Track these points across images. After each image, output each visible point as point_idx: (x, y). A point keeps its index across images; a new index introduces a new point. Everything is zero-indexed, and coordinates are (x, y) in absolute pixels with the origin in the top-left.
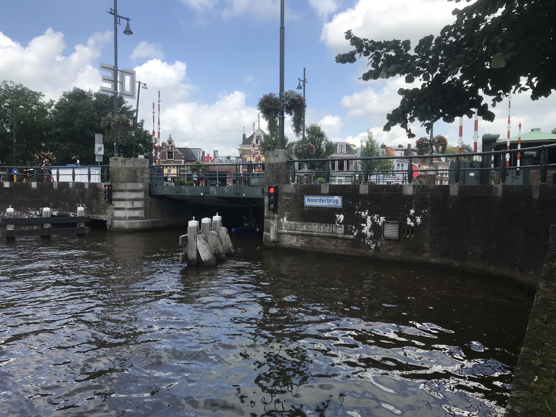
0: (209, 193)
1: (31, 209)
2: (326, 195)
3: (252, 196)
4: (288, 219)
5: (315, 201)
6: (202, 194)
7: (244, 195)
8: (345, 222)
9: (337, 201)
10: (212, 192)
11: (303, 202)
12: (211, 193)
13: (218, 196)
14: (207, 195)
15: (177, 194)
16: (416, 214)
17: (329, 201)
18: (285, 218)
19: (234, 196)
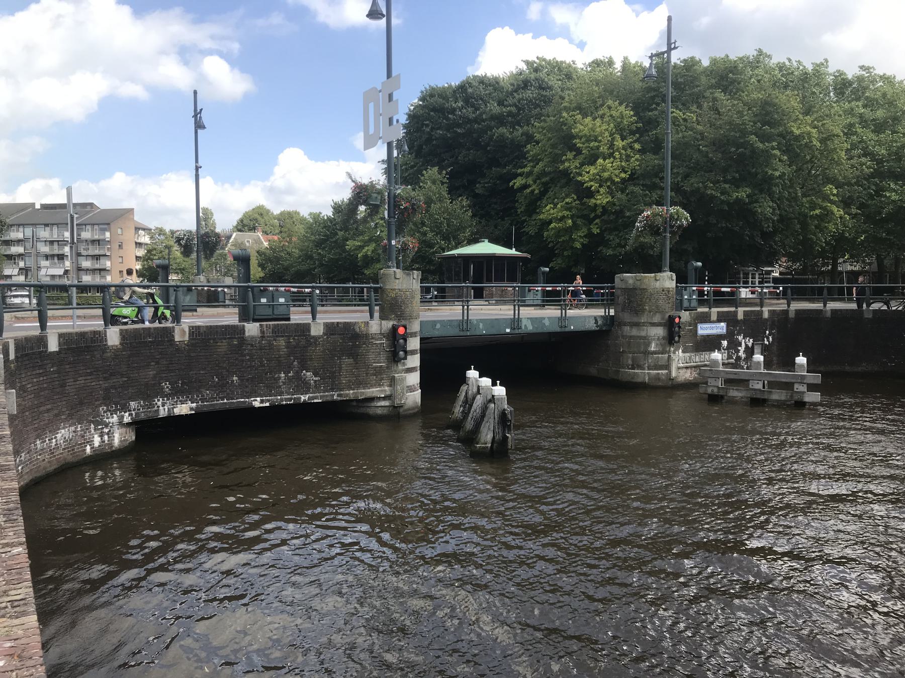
0: (521, 328)
1: (108, 410)
2: (714, 322)
3: (583, 329)
4: (683, 352)
5: (706, 329)
6: (508, 330)
7: (572, 327)
8: (728, 348)
9: (702, 328)
10: (526, 326)
11: (696, 331)
12: (523, 328)
13: (535, 331)
14: (517, 331)
15: (462, 334)
16: (770, 334)
17: (717, 328)
18: (680, 350)
19: (558, 330)
